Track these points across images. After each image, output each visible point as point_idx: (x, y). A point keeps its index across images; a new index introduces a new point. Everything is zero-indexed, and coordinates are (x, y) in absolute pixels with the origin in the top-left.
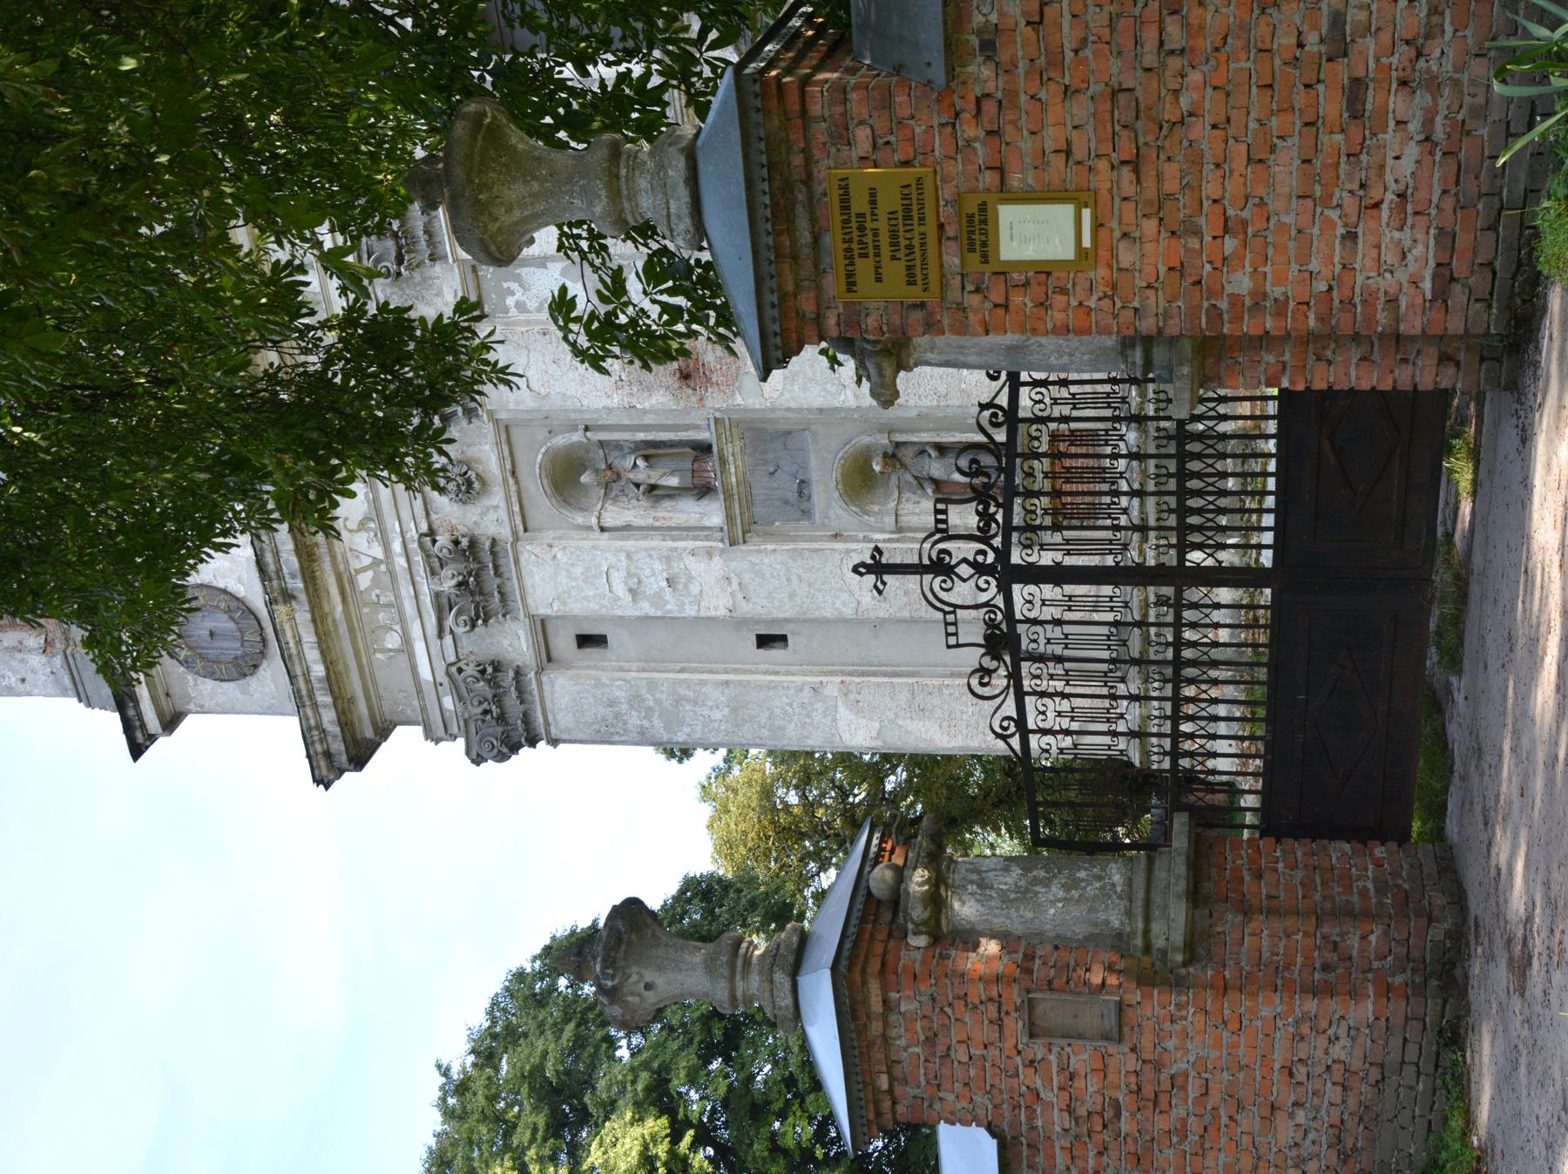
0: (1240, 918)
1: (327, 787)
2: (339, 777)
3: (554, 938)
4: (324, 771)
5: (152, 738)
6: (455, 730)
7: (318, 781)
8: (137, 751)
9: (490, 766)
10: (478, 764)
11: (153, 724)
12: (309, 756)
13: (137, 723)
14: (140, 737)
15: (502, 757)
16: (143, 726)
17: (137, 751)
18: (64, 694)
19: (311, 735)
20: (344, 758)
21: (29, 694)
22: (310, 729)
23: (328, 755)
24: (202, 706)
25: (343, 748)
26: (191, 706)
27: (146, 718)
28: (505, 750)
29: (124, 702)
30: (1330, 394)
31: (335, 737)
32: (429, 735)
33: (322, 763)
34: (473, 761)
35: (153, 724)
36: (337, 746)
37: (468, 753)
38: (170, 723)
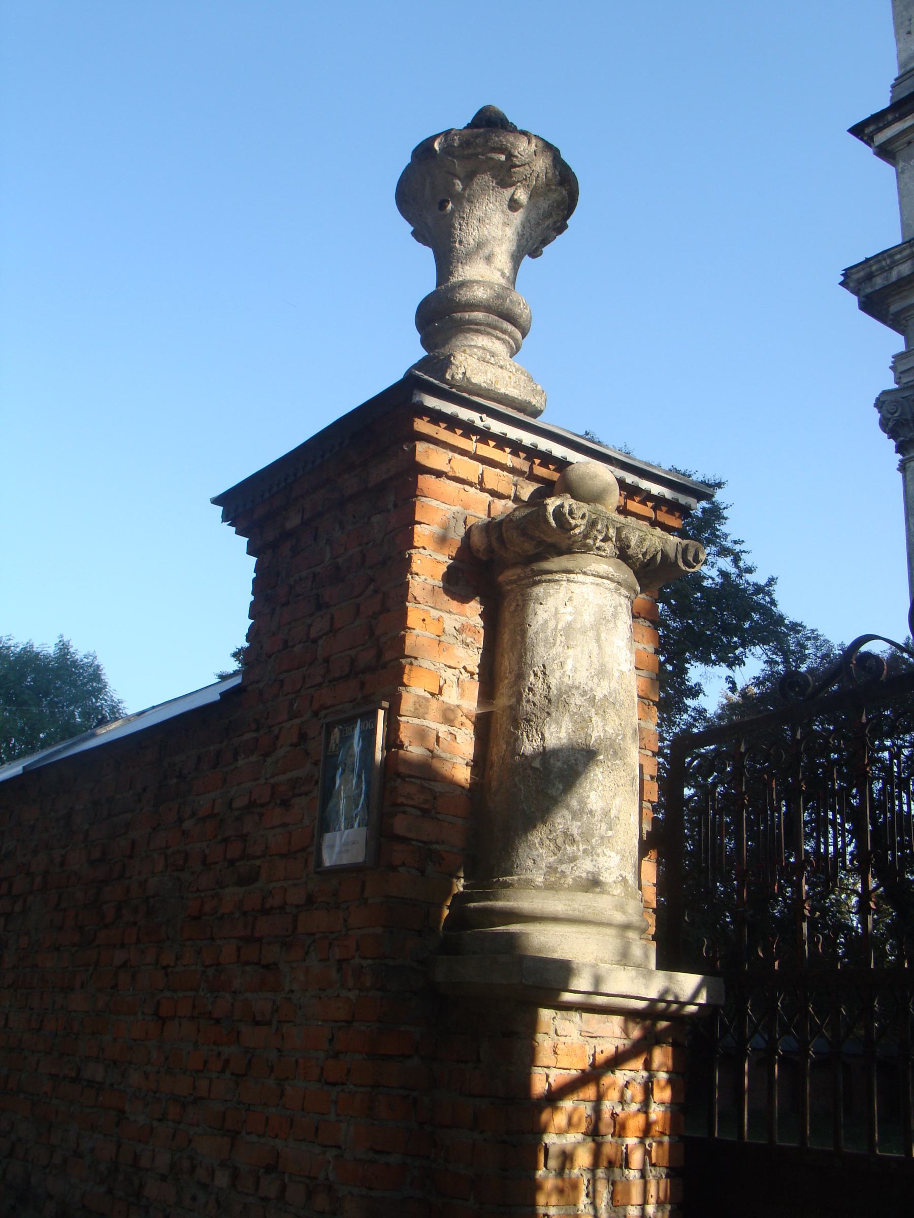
0: (516, 197)
1: (841, 284)
2: (853, 292)
3: (654, 885)
4: (855, 277)
5: (869, 141)
6: (904, 380)
7: (847, 273)
8: (858, 131)
9: (876, 416)
10: (876, 405)
11: (880, 138)
12: (867, 260)
13: (881, 125)
14: (868, 130)
15: (884, 425)
16: (880, 130)
17: (858, 131)
18: (901, 65)
19: (885, 259)
20: (869, 290)
21: (898, 40)
22: (891, 256)
23: (870, 277)
24: (902, 172)
25: (878, 288)
26: (901, 164)
27: (886, 130)
28: (890, 424)
29: (902, 106)
30: (659, 840)
31: (887, 278)
32: (898, 358)
33: (862, 274)
34: (878, 399)
35: (880, 138)
36: (879, 282)
37: (884, 393)
38: (885, 152)
